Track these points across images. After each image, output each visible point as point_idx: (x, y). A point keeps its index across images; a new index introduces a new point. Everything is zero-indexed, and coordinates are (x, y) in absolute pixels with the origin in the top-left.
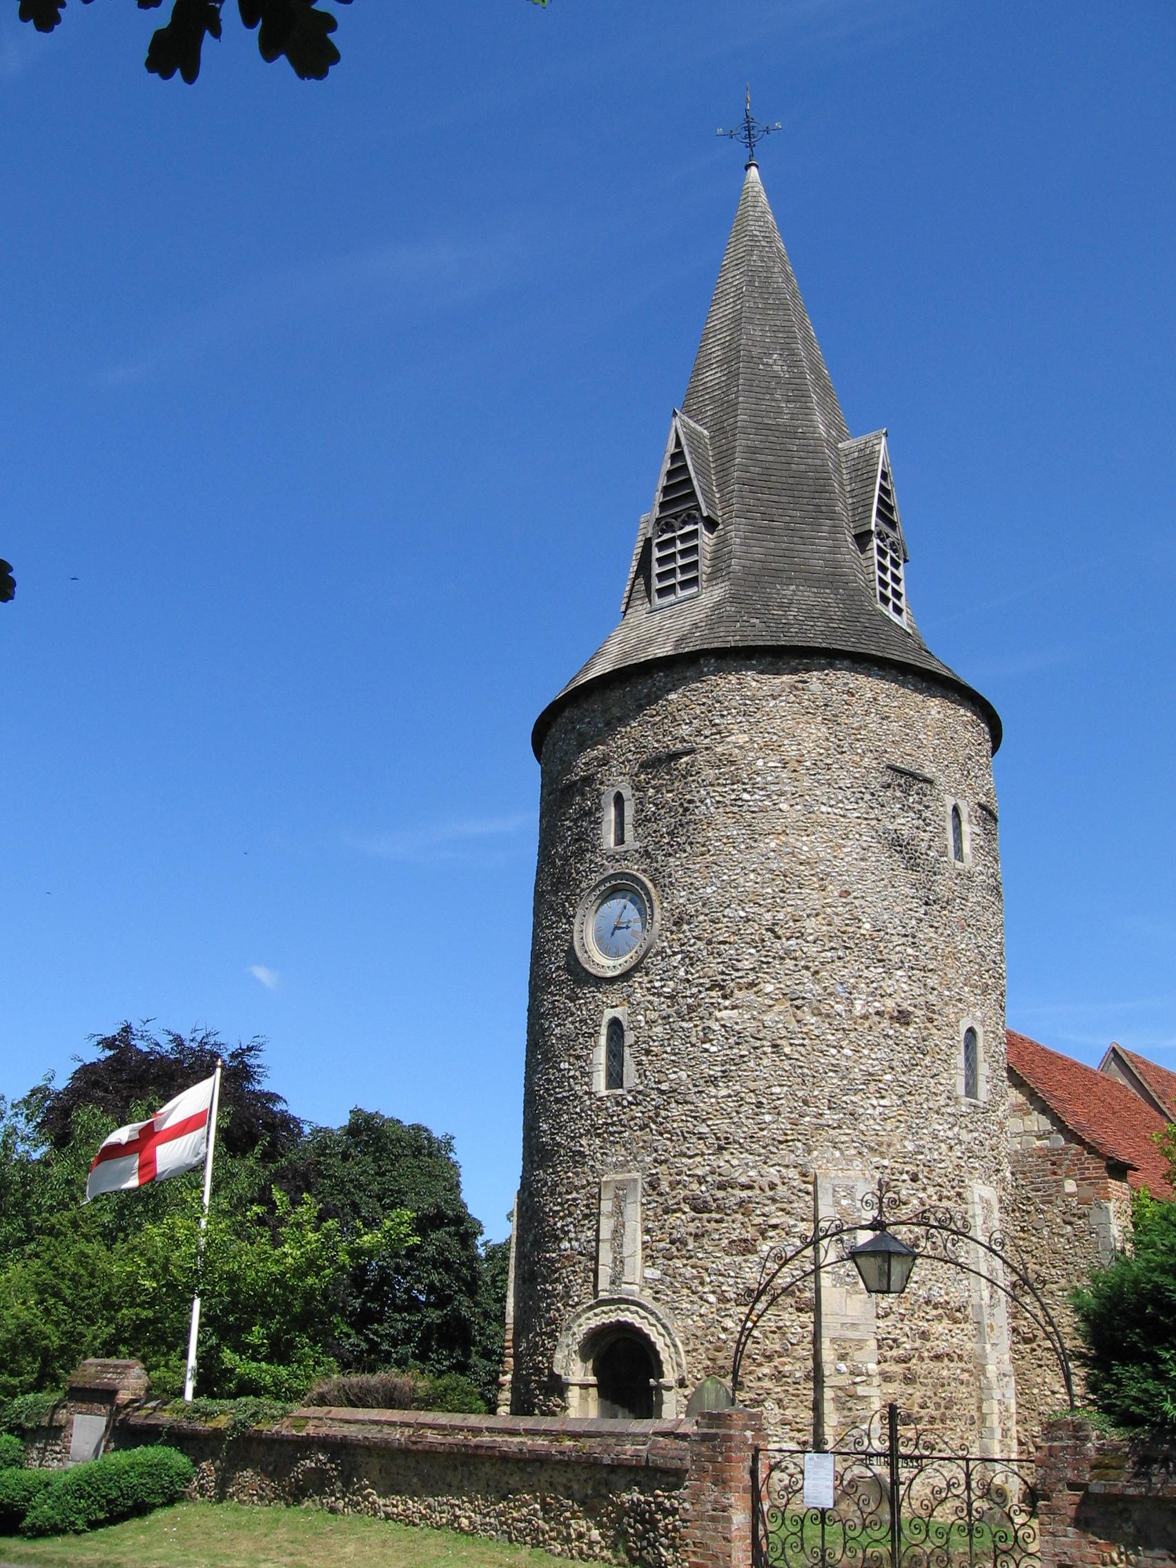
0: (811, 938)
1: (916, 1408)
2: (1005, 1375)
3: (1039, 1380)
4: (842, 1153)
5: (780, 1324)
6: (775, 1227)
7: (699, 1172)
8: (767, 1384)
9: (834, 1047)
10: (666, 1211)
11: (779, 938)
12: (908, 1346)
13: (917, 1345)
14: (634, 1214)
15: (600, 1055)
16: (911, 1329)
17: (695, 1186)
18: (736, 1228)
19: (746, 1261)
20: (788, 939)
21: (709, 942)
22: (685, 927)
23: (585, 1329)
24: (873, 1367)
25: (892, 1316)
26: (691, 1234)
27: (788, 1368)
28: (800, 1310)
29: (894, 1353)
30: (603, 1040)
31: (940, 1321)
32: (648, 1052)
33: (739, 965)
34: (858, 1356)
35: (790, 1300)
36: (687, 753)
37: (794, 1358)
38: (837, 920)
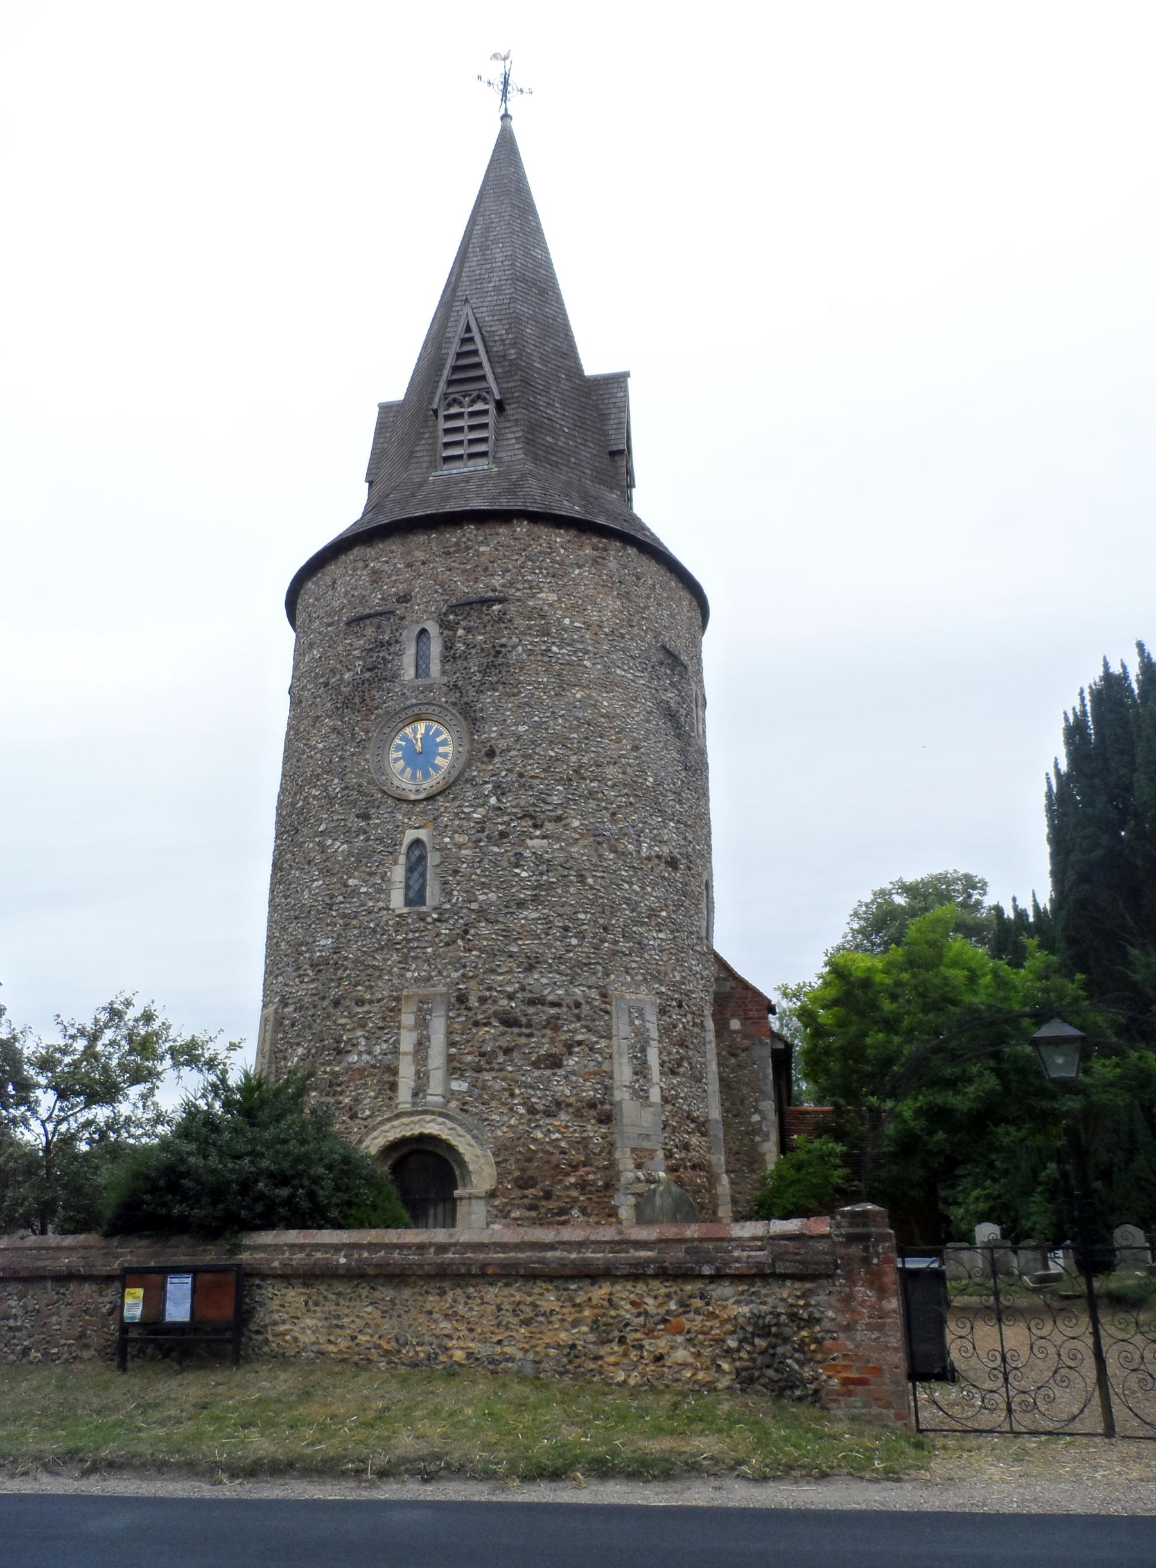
0: (609, 783)
4: (632, 978)
5: (585, 1135)
6: (579, 1043)
7: (509, 989)
8: (574, 1193)
10: (476, 1024)
11: (584, 779)
15: (398, 873)
17: (505, 1002)
19: (554, 1074)
20: (591, 781)
21: (521, 775)
22: (496, 760)
26: (501, 1047)
28: (600, 1121)
32: (456, 872)
33: (549, 799)
34: (649, 1164)
35: (593, 1112)
36: (500, 601)
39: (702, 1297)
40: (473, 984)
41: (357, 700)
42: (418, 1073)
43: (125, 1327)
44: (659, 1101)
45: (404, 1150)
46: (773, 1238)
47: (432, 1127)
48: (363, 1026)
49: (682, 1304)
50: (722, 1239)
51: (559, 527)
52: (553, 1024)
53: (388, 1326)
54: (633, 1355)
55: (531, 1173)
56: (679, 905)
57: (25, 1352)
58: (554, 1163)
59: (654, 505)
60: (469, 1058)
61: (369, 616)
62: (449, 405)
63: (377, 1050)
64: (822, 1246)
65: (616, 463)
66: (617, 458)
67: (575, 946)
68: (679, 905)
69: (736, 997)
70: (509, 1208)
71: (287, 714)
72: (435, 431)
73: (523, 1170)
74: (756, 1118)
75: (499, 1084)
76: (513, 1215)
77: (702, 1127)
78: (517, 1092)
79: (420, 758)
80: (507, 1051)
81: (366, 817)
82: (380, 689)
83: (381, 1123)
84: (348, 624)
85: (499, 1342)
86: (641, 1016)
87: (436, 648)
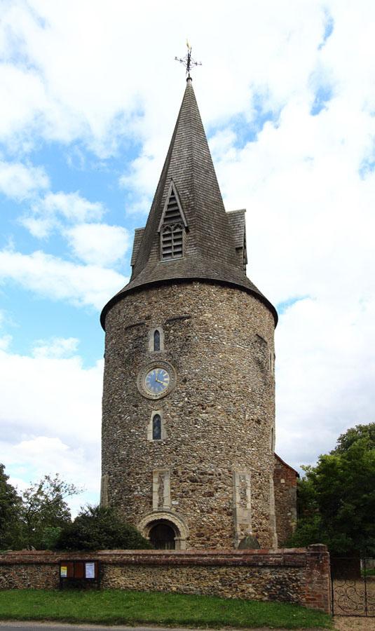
6: (220, 488)
8: (218, 539)
10: (181, 482)
14: (167, 483)
15: (150, 427)
18: (207, 488)
21: (197, 389)
22: (187, 383)
28: (228, 515)
32: (172, 427)
33: (208, 398)
35: (225, 512)
38: (241, 386)
39: (258, 573)
40: (179, 467)
41: (131, 360)
42: (160, 498)
43: (61, 579)
44: (250, 508)
45: (155, 525)
46: (284, 554)
47: (166, 517)
48: (138, 483)
49: (251, 574)
50: (266, 554)
51: (213, 285)
52: (210, 481)
53: (150, 579)
54: (234, 590)
55: (202, 532)
56: (260, 438)
57: (29, 585)
59: (256, 274)
60: (179, 493)
61: (134, 326)
62: (165, 230)
63: (144, 490)
64: (302, 557)
65: (239, 253)
66: (240, 251)
68: (260, 438)
69: (283, 470)
71: (104, 366)
72: (159, 242)
73: (199, 531)
77: (267, 517)
79: (155, 383)
80: (192, 491)
81: (136, 406)
82: (140, 355)
83: (147, 515)
84: (126, 329)
85: (188, 585)
86: (244, 478)
87: (162, 338)
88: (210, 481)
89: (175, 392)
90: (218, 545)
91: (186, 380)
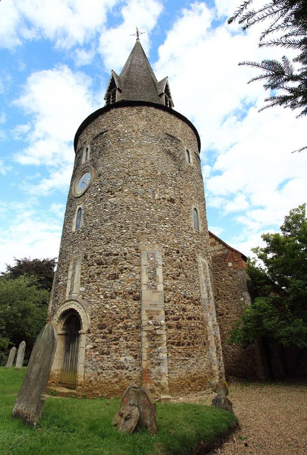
1: (182, 339)
2: (215, 325)
3: (226, 328)
4: (151, 243)
5: (127, 305)
6: (126, 269)
7: (100, 251)
8: (121, 331)
9: (148, 208)
10: (89, 266)
12: (178, 314)
13: (182, 313)
14: (78, 268)
16: (179, 307)
18: (112, 270)
19: (115, 282)
20: (133, 176)
21: (108, 179)
23: (60, 313)
24: (163, 322)
25: (171, 302)
27: (129, 323)
28: (135, 300)
29: (172, 316)
30: (76, 215)
31: (190, 304)
33: (117, 185)
34: (157, 317)
35: (131, 296)
36: (105, 132)
37: (132, 319)
42: (71, 285)
52: (115, 262)
55: (103, 322)
58: (113, 318)
60: (86, 278)
67: (125, 233)
69: (226, 257)
70: (95, 338)
73: (101, 321)
74: (242, 299)
75: (94, 287)
76: (96, 341)
77: (196, 302)
78: (101, 289)
86: (154, 255)
88: (115, 262)
89: (93, 186)
90: (121, 339)
91: (100, 174)
